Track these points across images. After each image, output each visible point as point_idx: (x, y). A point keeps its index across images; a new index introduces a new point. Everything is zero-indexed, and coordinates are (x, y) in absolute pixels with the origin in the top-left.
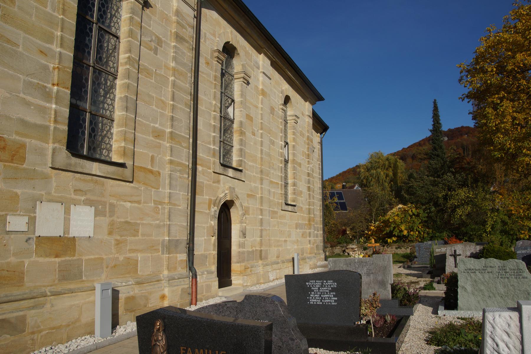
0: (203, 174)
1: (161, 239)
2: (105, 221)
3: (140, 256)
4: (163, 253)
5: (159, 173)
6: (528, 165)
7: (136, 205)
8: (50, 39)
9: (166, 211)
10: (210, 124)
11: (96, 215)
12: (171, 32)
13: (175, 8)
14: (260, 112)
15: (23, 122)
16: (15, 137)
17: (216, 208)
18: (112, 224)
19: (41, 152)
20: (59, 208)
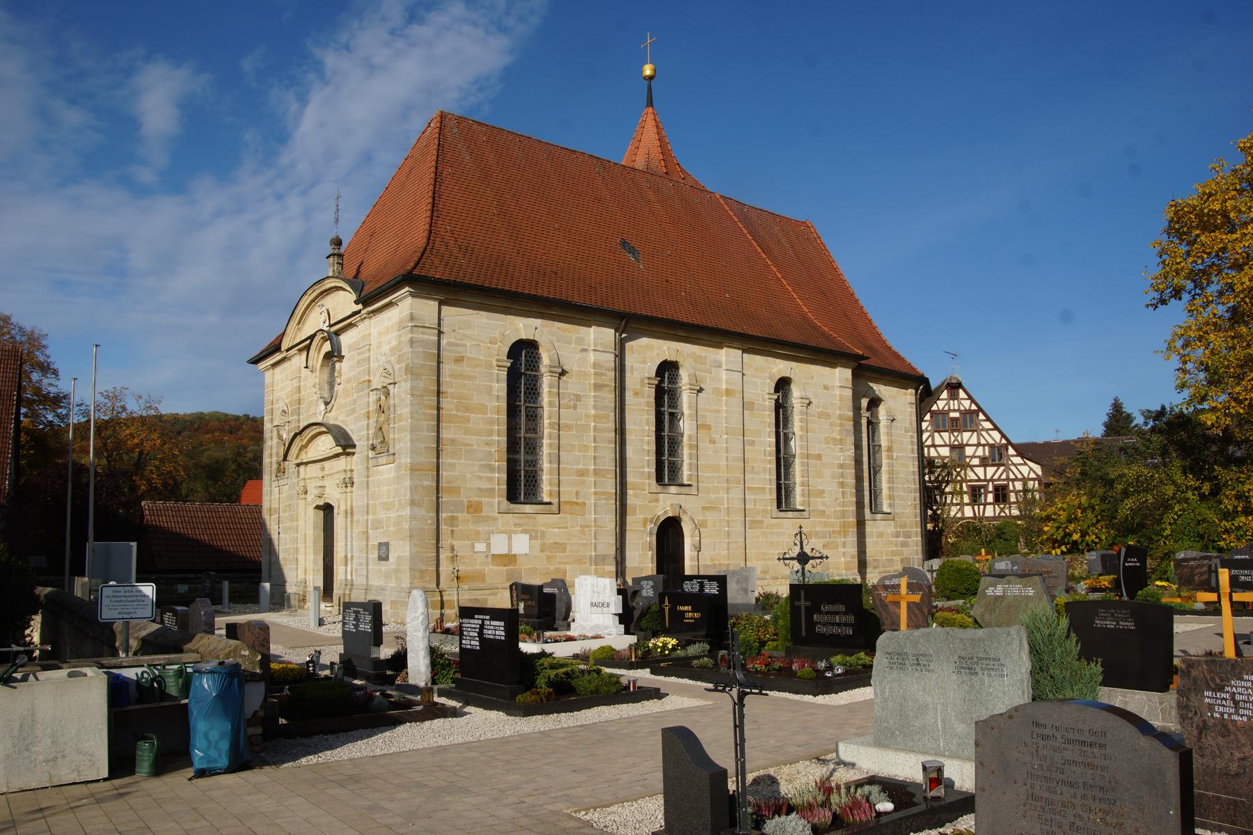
0: (635, 496)
1: (589, 554)
2: (537, 543)
3: (568, 567)
4: (591, 565)
5: (585, 504)
6: (1251, 355)
7: (563, 530)
8: (490, 433)
9: (593, 532)
10: (644, 450)
11: (530, 539)
12: (590, 384)
13: (592, 361)
14: (725, 415)
15: (480, 489)
16: (476, 499)
17: (652, 525)
18: (543, 544)
19: (491, 505)
20: (504, 537)
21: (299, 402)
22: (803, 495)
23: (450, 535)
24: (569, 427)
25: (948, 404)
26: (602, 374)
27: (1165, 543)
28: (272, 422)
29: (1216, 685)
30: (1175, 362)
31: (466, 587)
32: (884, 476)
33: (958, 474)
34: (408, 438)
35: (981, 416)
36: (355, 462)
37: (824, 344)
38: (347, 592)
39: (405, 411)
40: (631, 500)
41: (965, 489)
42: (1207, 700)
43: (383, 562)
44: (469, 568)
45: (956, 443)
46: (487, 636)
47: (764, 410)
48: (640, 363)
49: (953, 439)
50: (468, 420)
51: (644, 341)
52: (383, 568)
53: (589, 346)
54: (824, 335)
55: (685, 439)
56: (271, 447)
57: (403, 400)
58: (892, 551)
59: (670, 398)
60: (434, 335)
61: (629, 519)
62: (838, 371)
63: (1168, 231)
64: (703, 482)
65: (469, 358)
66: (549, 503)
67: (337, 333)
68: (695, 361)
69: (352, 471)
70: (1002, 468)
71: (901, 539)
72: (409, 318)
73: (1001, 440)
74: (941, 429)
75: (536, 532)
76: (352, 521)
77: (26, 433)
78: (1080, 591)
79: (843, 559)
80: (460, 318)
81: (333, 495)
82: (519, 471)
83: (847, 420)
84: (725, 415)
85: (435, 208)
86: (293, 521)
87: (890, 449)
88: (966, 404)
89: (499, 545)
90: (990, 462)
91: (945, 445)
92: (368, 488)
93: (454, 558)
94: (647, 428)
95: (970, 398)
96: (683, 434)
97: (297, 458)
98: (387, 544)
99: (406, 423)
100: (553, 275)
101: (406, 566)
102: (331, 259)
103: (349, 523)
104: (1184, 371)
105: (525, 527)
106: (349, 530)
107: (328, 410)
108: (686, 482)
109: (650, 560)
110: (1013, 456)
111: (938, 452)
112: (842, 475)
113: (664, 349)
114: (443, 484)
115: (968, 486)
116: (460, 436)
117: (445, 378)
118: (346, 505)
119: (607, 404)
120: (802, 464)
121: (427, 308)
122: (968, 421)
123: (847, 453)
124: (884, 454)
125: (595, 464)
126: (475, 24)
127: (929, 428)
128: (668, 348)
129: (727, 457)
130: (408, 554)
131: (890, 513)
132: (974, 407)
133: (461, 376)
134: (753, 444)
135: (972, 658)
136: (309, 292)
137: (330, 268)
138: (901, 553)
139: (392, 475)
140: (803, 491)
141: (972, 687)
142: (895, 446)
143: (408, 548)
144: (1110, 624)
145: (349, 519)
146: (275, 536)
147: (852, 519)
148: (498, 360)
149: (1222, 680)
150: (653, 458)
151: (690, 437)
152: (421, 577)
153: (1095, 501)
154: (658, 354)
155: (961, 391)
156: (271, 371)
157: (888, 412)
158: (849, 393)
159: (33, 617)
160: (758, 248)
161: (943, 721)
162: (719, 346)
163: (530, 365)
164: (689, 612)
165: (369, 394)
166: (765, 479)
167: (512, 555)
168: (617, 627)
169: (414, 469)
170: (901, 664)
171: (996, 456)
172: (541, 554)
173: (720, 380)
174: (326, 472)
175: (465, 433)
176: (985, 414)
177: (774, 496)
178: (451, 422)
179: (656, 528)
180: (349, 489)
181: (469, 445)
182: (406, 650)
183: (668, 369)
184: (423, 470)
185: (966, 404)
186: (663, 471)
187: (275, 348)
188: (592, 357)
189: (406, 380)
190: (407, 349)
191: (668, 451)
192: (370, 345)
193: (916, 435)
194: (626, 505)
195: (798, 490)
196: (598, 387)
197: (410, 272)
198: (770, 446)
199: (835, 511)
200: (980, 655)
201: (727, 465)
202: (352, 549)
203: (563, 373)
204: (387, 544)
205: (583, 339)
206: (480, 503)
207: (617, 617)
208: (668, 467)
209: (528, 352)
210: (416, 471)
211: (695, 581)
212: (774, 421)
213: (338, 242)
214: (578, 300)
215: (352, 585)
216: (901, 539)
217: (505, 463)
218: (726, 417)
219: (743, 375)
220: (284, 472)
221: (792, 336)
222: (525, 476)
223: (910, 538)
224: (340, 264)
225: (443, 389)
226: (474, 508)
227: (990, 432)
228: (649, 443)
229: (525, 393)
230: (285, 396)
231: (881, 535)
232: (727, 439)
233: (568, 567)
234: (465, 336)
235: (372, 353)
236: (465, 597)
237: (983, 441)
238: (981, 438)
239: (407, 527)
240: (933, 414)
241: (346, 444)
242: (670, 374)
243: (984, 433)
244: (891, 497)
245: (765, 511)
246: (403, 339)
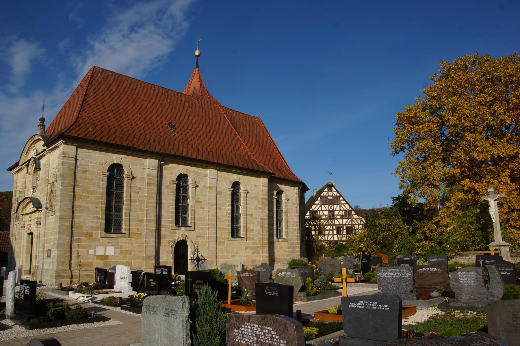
0: (165, 231)
1: (142, 255)
2: (118, 250)
3: (132, 261)
5: (141, 234)
8: (98, 203)
12: (146, 183)
14: (208, 197)
15: (92, 227)
16: (90, 231)
19: (97, 234)
20: (103, 248)
21: (25, 188)
22: (244, 231)
23: (77, 247)
24: (135, 201)
25: (328, 193)
26: (151, 179)
27: (395, 252)
28: (16, 196)
29: (237, 326)
30: (398, 178)
31: (84, 269)
32: (284, 224)
33: (332, 222)
34: (59, 204)
35: (341, 198)
36: (41, 215)
37: (255, 168)
38: (35, 271)
39: (59, 193)
40: (163, 232)
41: (334, 228)
42: (235, 333)
43: (49, 258)
44: (86, 261)
45: (331, 209)
46: (26, 293)
47: (227, 195)
48: (169, 174)
49: (329, 207)
50: (88, 197)
51: (172, 165)
52: (49, 261)
53: (146, 166)
54: (257, 164)
55: (190, 207)
56: (15, 207)
57: (58, 188)
58: (286, 255)
59: (183, 190)
60: (74, 161)
61: (162, 241)
62: (261, 179)
63: (398, 124)
64: (197, 225)
65: (90, 171)
66: (125, 233)
67: (39, 159)
68: (195, 174)
69: (40, 218)
70: (350, 220)
71: (291, 250)
72: (62, 153)
73: (349, 208)
74: (325, 203)
75: (118, 246)
76: (39, 240)
78: (350, 273)
79: (262, 258)
80: (86, 154)
81: (34, 229)
82: (112, 219)
83: (265, 200)
84: (208, 197)
85: (82, 107)
86: (20, 240)
87: (286, 212)
88: (335, 193)
89: (100, 251)
90: (345, 217)
91: (326, 210)
92: (45, 226)
93: (78, 257)
94: (172, 202)
95: (337, 191)
96: (189, 205)
97: (22, 212)
98: (50, 250)
99: (58, 198)
100: (133, 136)
101: (55, 260)
102: (39, 127)
103: (38, 241)
104: (403, 182)
105: (113, 244)
106: (38, 244)
107: (34, 192)
108: (189, 225)
109: (171, 259)
110: (354, 215)
111: (323, 213)
112: (262, 223)
113: (181, 169)
114: (75, 224)
115: (336, 227)
116: (84, 204)
117: (78, 179)
118: (37, 233)
119: (153, 192)
120: (244, 218)
121: (71, 149)
122: (336, 200)
123: (265, 214)
124: (284, 214)
125: (146, 217)
126: (159, 35)
127: (320, 203)
128: (183, 168)
129: (208, 215)
131: (286, 239)
132: (338, 195)
133: (86, 178)
134: (221, 209)
135: (168, 310)
136: (30, 141)
137: (38, 131)
138: (291, 256)
139: (53, 220)
140: (244, 229)
141: (168, 322)
142: (289, 211)
144: (270, 293)
145: (38, 239)
146: (14, 246)
147: (266, 241)
148: (103, 172)
149: (239, 325)
150: (174, 215)
151: (191, 206)
152: (62, 265)
153: (371, 234)
154: (178, 171)
155: (333, 188)
156: (16, 174)
157: (286, 196)
158: (266, 188)
160: (233, 127)
161: (160, 337)
162: (207, 168)
163: (119, 174)
164: (153, 282)
165: (48, 185)
166: (226, 224)
167: (106, 256)
168: (129, 288)
169: (61, 218)
170: (149, 311)
171: (347, 215)
172: (120, 255)
173: (206, 182)
174: (32, 218)
175: (86, 203)
176: (343, 198)
177: (230, 231)
178: (80, 198)
179: (174, 245)
180: (39, 226)
181: (88, 208)
182: (109, 293)
183: (182, 178)
184: (65, 218)
185: (335, 193)
186: (179, 220)
187: (17, 164)
188: (147, 171)
189: (60, 180)
190: (61, 167)
191: (182, 212)
192: (50, 164)
193: (298, 206)
194: (160, 235)
195: (242, 229)
196: (149, 184)
197: (63, 133)
198: (229, 210)
199: (259, 238)
200: (171, 309)
201: (208, 218)
202: (39, 252)
203: (133, 178)
204: (50, 250)
205: (143, 164)
206: (92, 233)
207: (130, 284)
208: (182, 219)
209: (118, 169)
210: (62, 218)
211: (160, 269)
212: (231, 200)
213: (43, 120)
214: (141, 147)
216: (291, 250)
217: (105, 216)
218: (209, 198)
219: (217, 180)
220: (18, 218)
221: (241, 164)
222: (114, 222)
223: (295, 249)
224: (43, 129)
225: (77, 184)
226: (89, 235)
227: (345, 205)
228: (172, 208)
229: (116, 186)
230: (21, 185)
231: (281, 248)
232: (209, 207)
233: (132, 261)
234: (88, 161)
235: (50, 168)
236: (82, 274)
237: (342, 209)
238: (341, 207)
239: (57, 243)
240: (322, 197)
241: (38, 205)
242: (184, 179)
243: (342, 205)
244: (287, 232)
245: (226, 238)
246: (60, 162)
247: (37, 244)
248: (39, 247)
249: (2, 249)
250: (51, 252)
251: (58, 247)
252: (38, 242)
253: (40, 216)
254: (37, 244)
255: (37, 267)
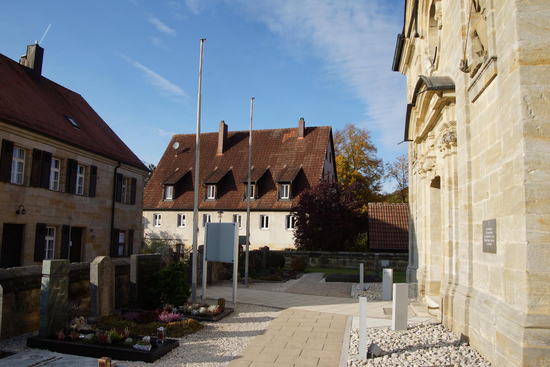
43: (489, 255)
52: (489, 265)
77: (354, 177)
103: (453, 196)
106: (454, 207)
118: (449, 172)
130: (523, 240)
143: (524, 229)
145: (453, 191)
159: (303, 274)
202: (457, 233)
210: (535, 63)
215: (457, 284)
239: (521, 184)
247: (450, 208)
248: (456, 215)
249: (397, 224)
250: (422, 76)
251: (527, 203)
252: (453, 202)
253: (453, 117)
254: (450, 208)
255: (454, 281)
